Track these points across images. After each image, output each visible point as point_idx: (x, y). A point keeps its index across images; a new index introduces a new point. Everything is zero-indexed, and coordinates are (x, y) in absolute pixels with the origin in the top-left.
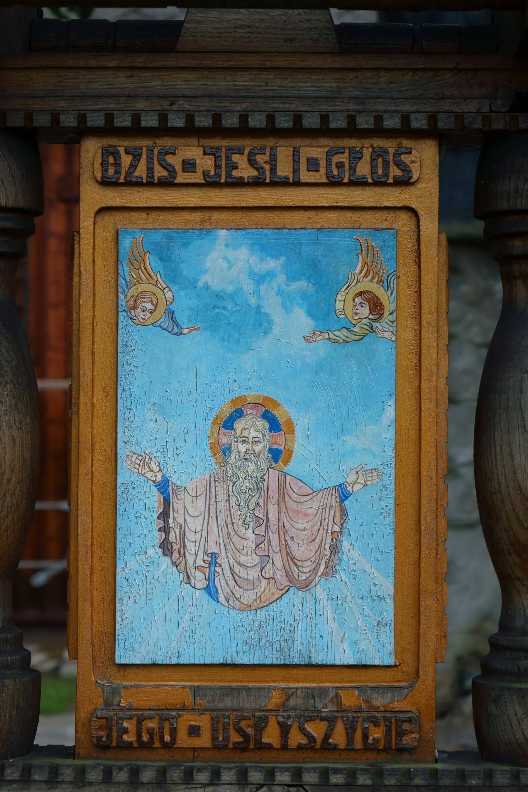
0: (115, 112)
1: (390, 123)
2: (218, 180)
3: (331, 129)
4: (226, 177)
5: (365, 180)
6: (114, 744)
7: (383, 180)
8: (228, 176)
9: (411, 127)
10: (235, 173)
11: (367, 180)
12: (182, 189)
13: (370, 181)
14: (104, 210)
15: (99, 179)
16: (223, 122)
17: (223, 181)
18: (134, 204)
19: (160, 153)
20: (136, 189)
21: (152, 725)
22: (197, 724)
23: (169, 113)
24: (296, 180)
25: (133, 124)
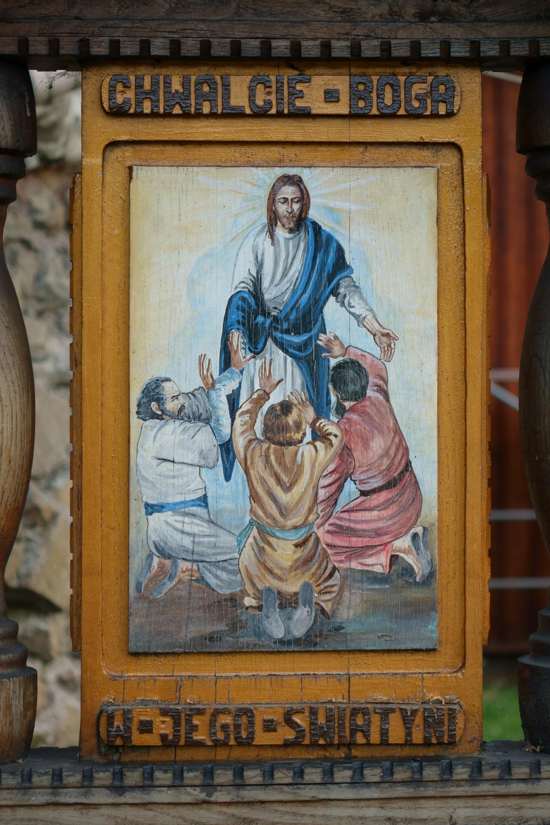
0: (242, 41)
1: (458, 51)
2: (367, 111)
3: (153, 56)
4: (223, 109)
5: (201, 111)
6: (182, 742)
7: (421, 111)
8: (291, 103)
9: (121, 54)
11: (143, 111)
12: (302, 120)
13: (248, 111)
14: (114, 144)
15: (107, 108)
16: (122, 50)
18: (438, 138)
19: (197, 84)
20: (136, 120)
21: (227, 720)
22: (148, 719)
23: (272, 41)
24: (435, 112)
25: (111, 52)
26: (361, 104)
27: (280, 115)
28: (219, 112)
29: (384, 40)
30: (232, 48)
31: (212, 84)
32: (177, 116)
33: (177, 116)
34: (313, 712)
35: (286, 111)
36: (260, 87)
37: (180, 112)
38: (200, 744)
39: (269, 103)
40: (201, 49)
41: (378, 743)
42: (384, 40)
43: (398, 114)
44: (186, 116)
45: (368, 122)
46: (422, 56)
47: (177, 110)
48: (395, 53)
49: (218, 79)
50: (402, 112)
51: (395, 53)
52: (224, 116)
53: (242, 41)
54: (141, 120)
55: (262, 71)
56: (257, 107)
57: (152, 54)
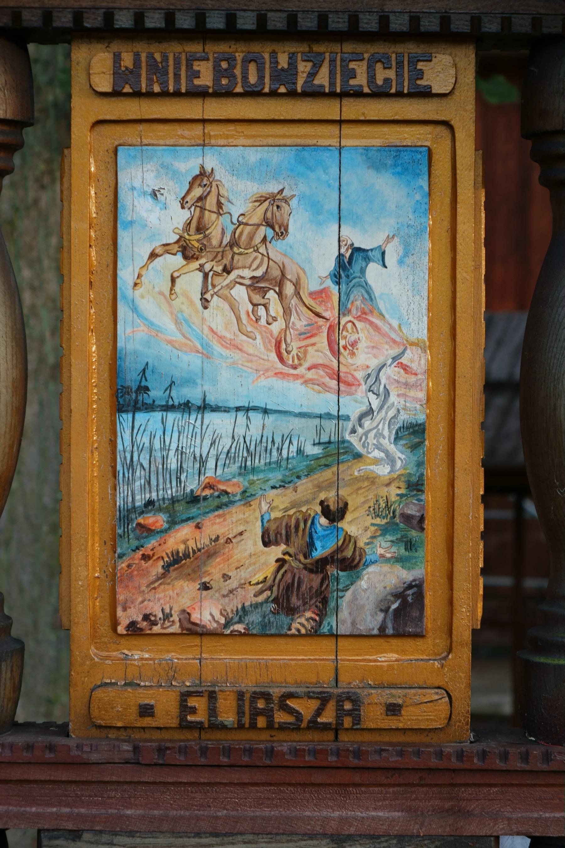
8: (345, 82)
10: (197, 82)
11: (431, 91)
13: (366, 90)
17: (393, 91)
19: (243, 61)
26: (224, 82)
27: (399, 95)
28: (406, 91)
29: (199, 11)
30: (288, 22)
31: (231, 60)
32: (282, 95)
33: (282, 95)
34: (212, 696)
35: (406, 91)
36: (379, 66)
37: (131, 91)
38: (223, 727)
39: (387, 81)
40: (380, 23)
41: (174, 725)
42: (199, 11)
43: (235, 91)
44: (137, 94)
45: (260, 100)
46: (361, 29)
47: (127, 89)
48: (454, 28)
49: (267, 56)
50: (239, 89)
51: (454, 28)
52: (410, 95)
53: (238, 13)
54: (361, 99)
55: (255, 47)
56: (377, 86)
57: (484, 30)
